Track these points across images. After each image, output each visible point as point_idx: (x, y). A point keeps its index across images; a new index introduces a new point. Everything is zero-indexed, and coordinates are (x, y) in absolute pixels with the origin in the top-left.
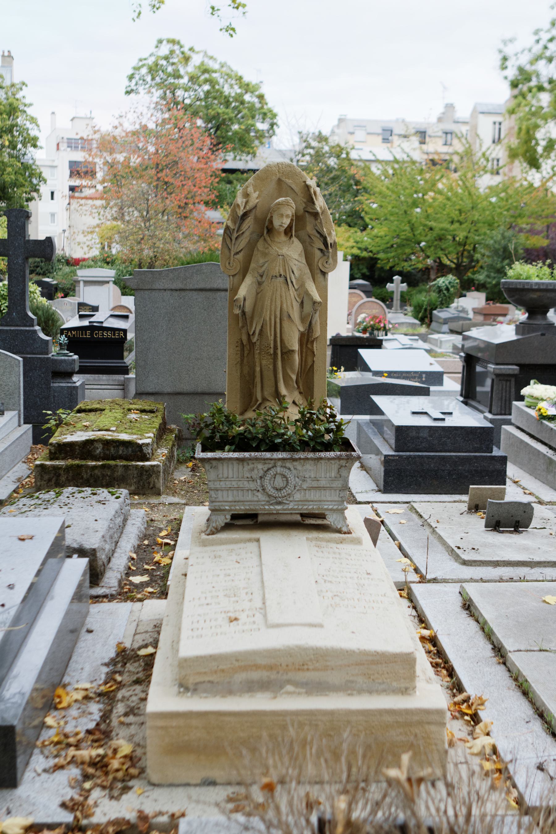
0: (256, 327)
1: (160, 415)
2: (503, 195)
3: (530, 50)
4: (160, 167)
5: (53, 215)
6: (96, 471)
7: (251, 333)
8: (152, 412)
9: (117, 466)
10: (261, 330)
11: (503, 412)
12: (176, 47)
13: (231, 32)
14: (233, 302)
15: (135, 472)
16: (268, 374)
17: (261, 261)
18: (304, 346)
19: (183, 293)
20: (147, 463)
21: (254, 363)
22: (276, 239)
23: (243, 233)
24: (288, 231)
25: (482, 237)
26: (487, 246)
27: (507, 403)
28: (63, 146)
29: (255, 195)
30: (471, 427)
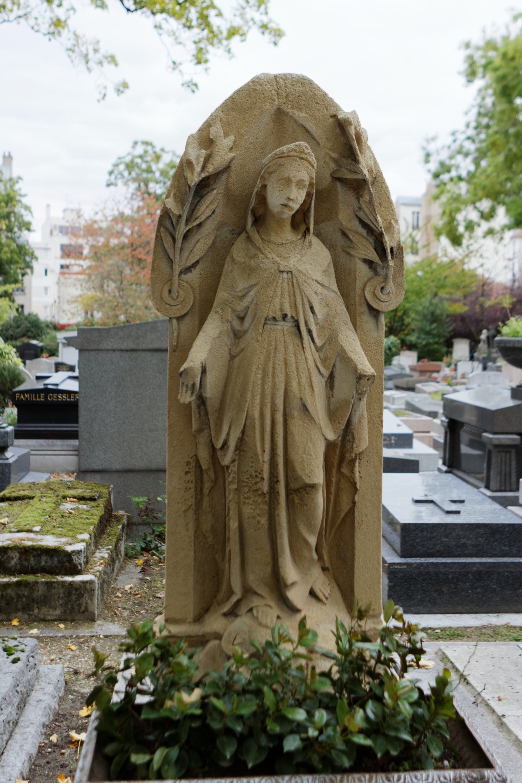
0: (230, 433)
1: (101, 503)
2: (427, 269)
3: (449, 147)
4: (134, 246)
5: (46, 289)
6: (9, 591)
7: (219, 445)
8: (92, 499)
9: (36, 583)
10: (241, 440)
11: (503, 488)
12: (149, 148)
13: (194, 88)
14: (178, 376)
15: (61, 591)
16: (258, 538)
17: (241, 285)
18: (334, 471)
19: (135, 355)
20: (78, 578)
21: (225, 509)
22: (274, 238)
23: (200, 225)
24: (300, 221)
25: (413, 304)
26: (417, 312)
27: (508, 478)
28: (56, 232)
29: (228, 142)
30: (498, 525)
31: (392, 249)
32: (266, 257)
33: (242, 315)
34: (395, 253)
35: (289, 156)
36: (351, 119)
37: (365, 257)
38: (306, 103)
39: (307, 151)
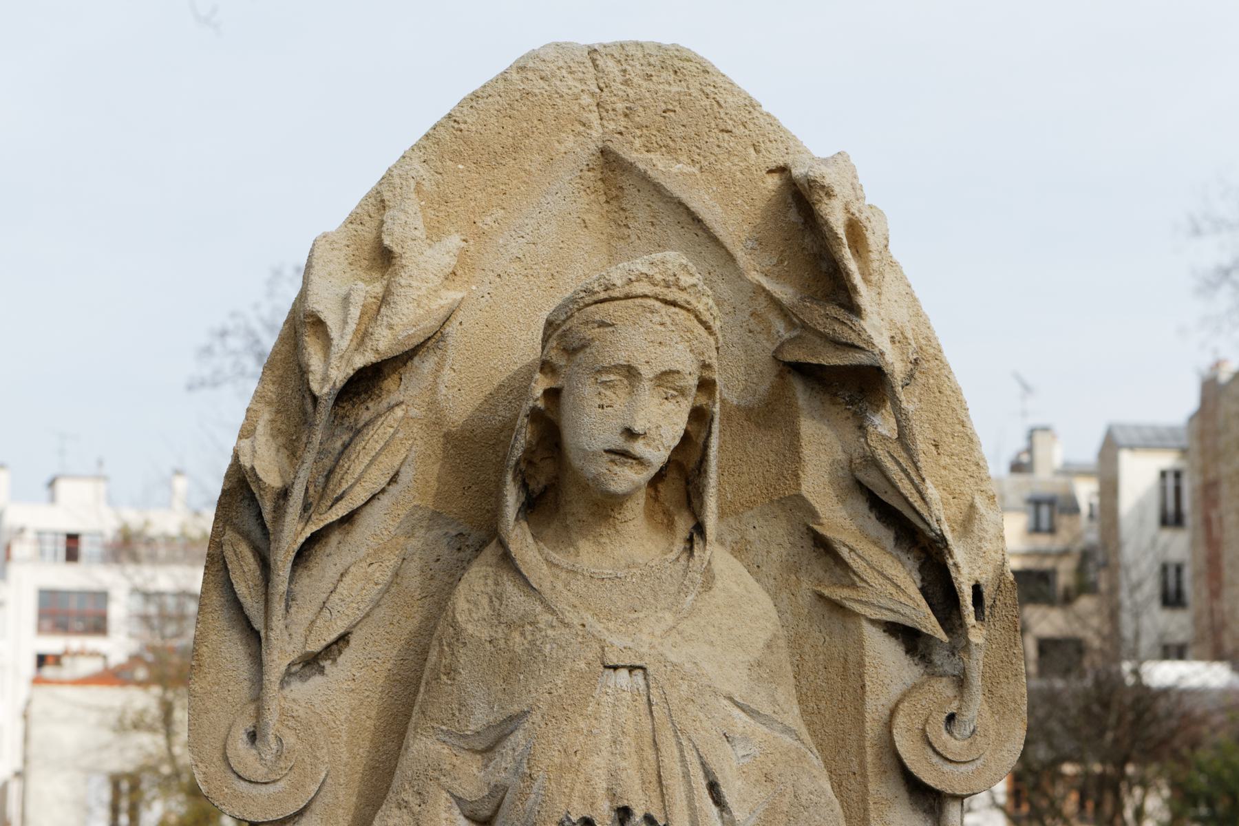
6: (935, 601)
23: (349, 519)
24: (682, 478)
31: (977, 589)
32: (562, 622)
33: (485, 812)
34: (988, 602)
35: (627, 297)
36: (830, 177)
37: (890, 617)
38: (691, 132)
39: (686, 280)
